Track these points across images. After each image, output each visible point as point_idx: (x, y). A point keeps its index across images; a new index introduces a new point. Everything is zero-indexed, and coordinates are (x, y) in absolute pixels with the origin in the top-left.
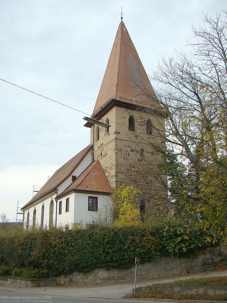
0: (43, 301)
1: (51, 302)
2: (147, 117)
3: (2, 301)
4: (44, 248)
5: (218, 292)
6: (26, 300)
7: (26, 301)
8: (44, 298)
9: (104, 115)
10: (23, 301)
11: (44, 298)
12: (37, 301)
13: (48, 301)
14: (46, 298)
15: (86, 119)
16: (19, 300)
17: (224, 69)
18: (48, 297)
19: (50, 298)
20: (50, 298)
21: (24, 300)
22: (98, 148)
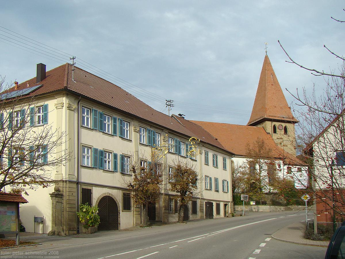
0: (49, 257)
1: (58, 257)
2: (284, 125)
3: (2, 257)
4: (61, 197)
5: (170, 141)
6: (30, 255)
7: (29, 257)
8: (51, 253)
9: (54, 70)
10: (26, 257)
11: (51, 253)
12: (42, 257)
13: (54, 257)
14: (55, 252)
15: (16, 83)
16: (22, 256)
17: (319, 167)
18: (52, 252)
19: (57, 253)
20: (57, 253)
21: (27, 256)
22: (277, 138)
